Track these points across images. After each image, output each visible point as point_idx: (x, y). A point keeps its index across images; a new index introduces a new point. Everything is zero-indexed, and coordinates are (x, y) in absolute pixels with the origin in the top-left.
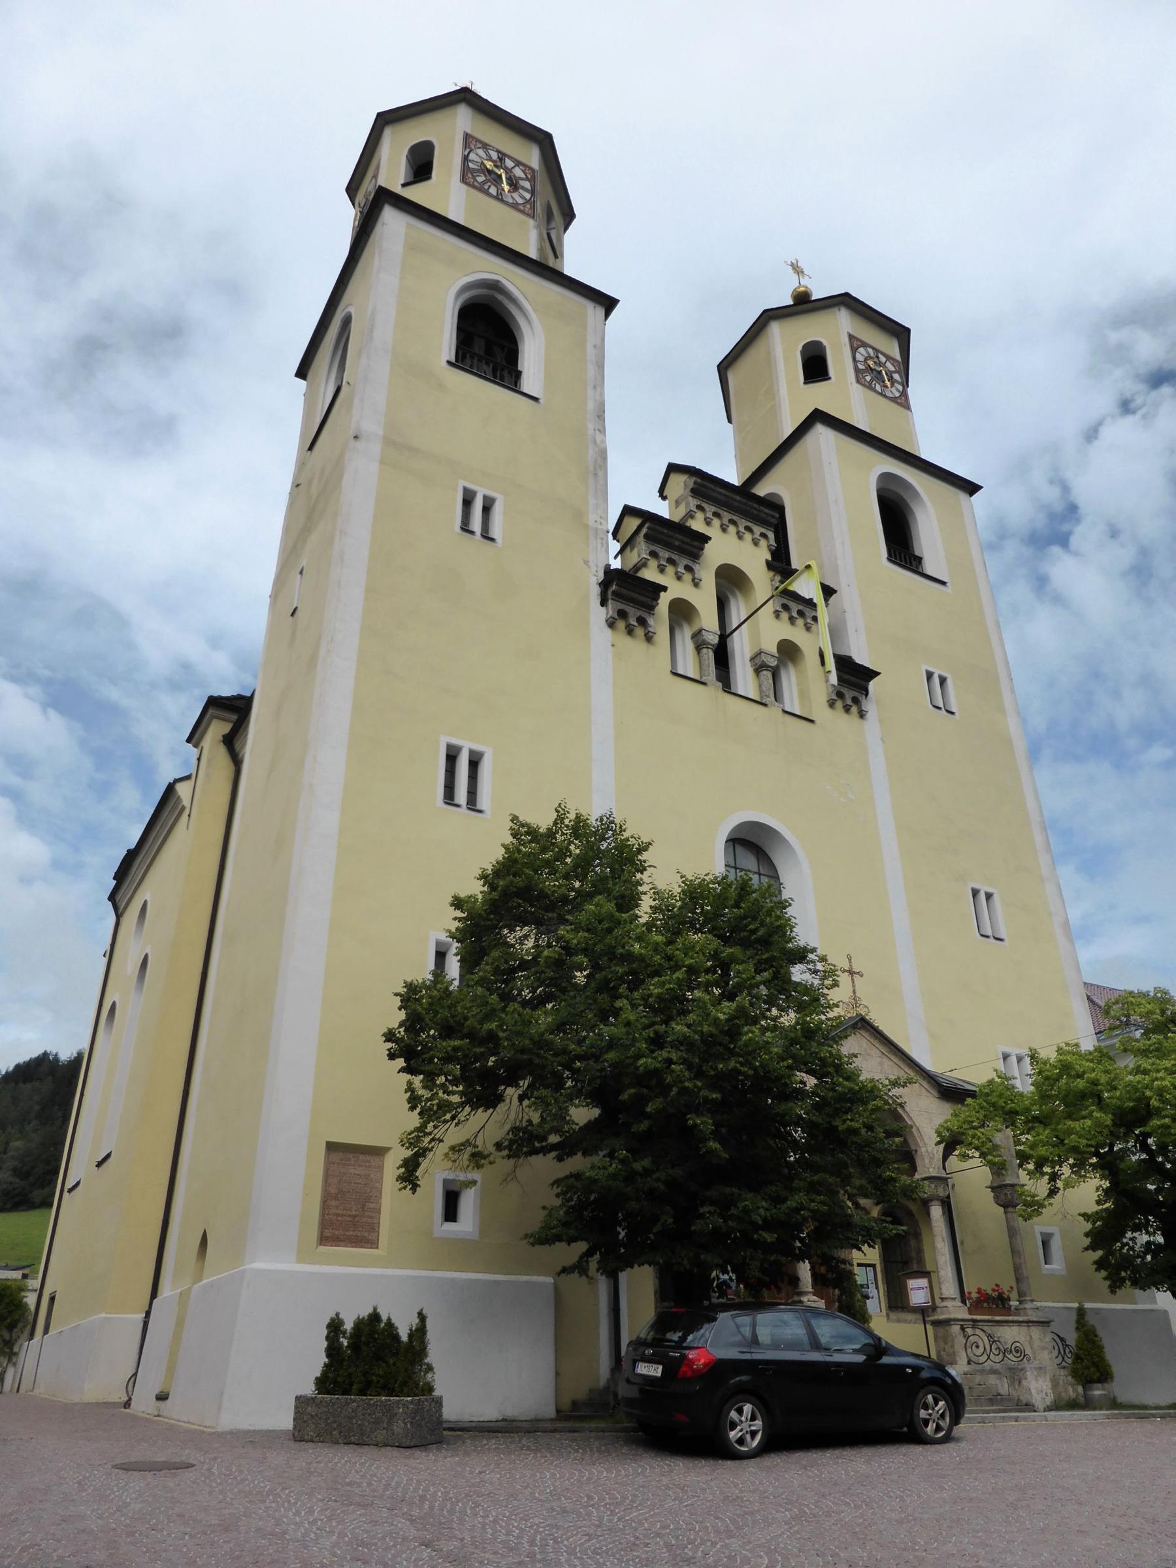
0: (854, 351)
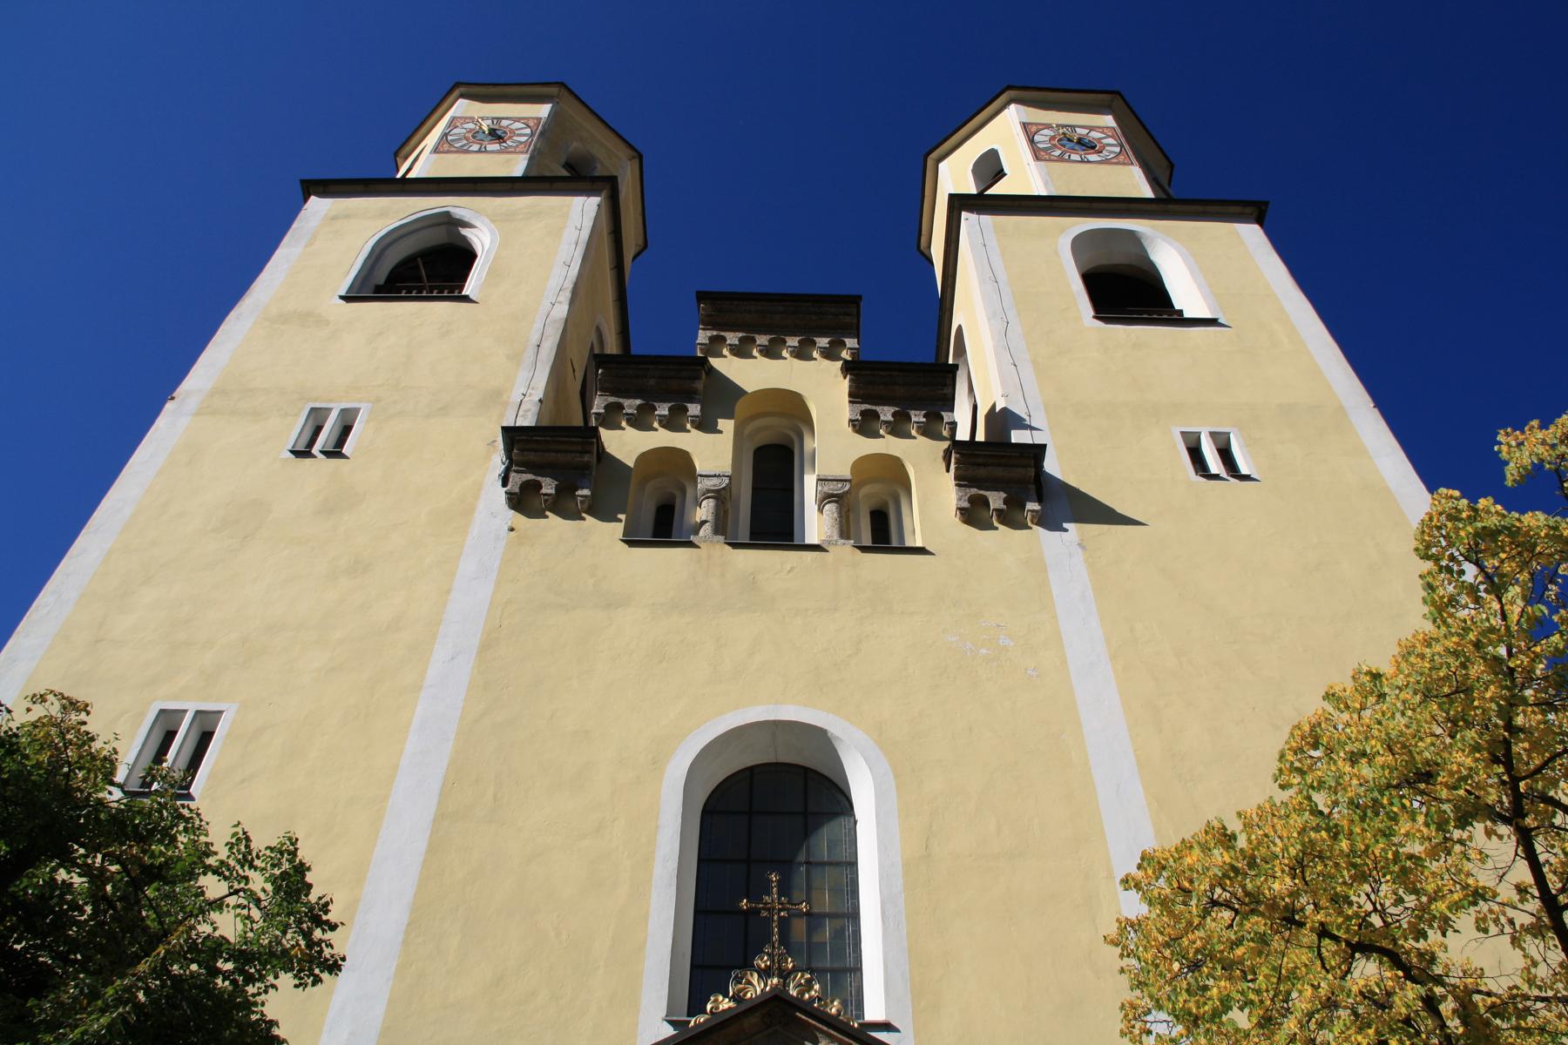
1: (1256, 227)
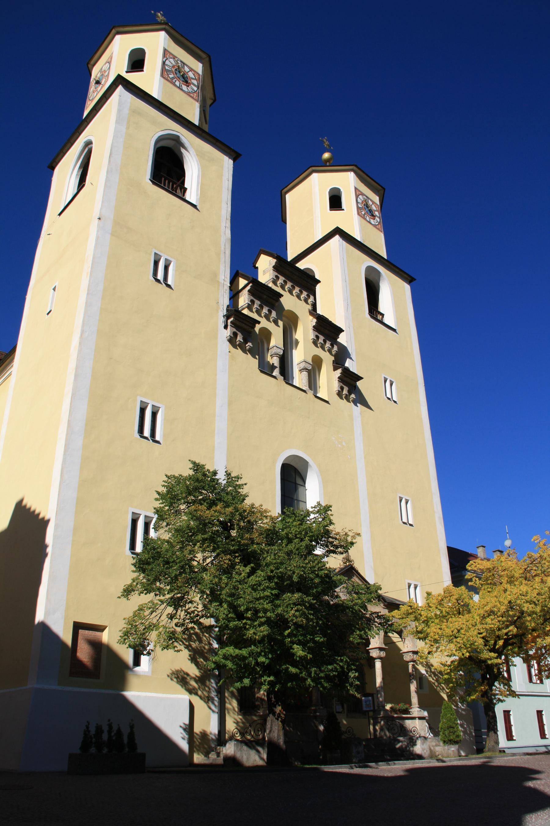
0: (357, 197)
1: (231, 162)
